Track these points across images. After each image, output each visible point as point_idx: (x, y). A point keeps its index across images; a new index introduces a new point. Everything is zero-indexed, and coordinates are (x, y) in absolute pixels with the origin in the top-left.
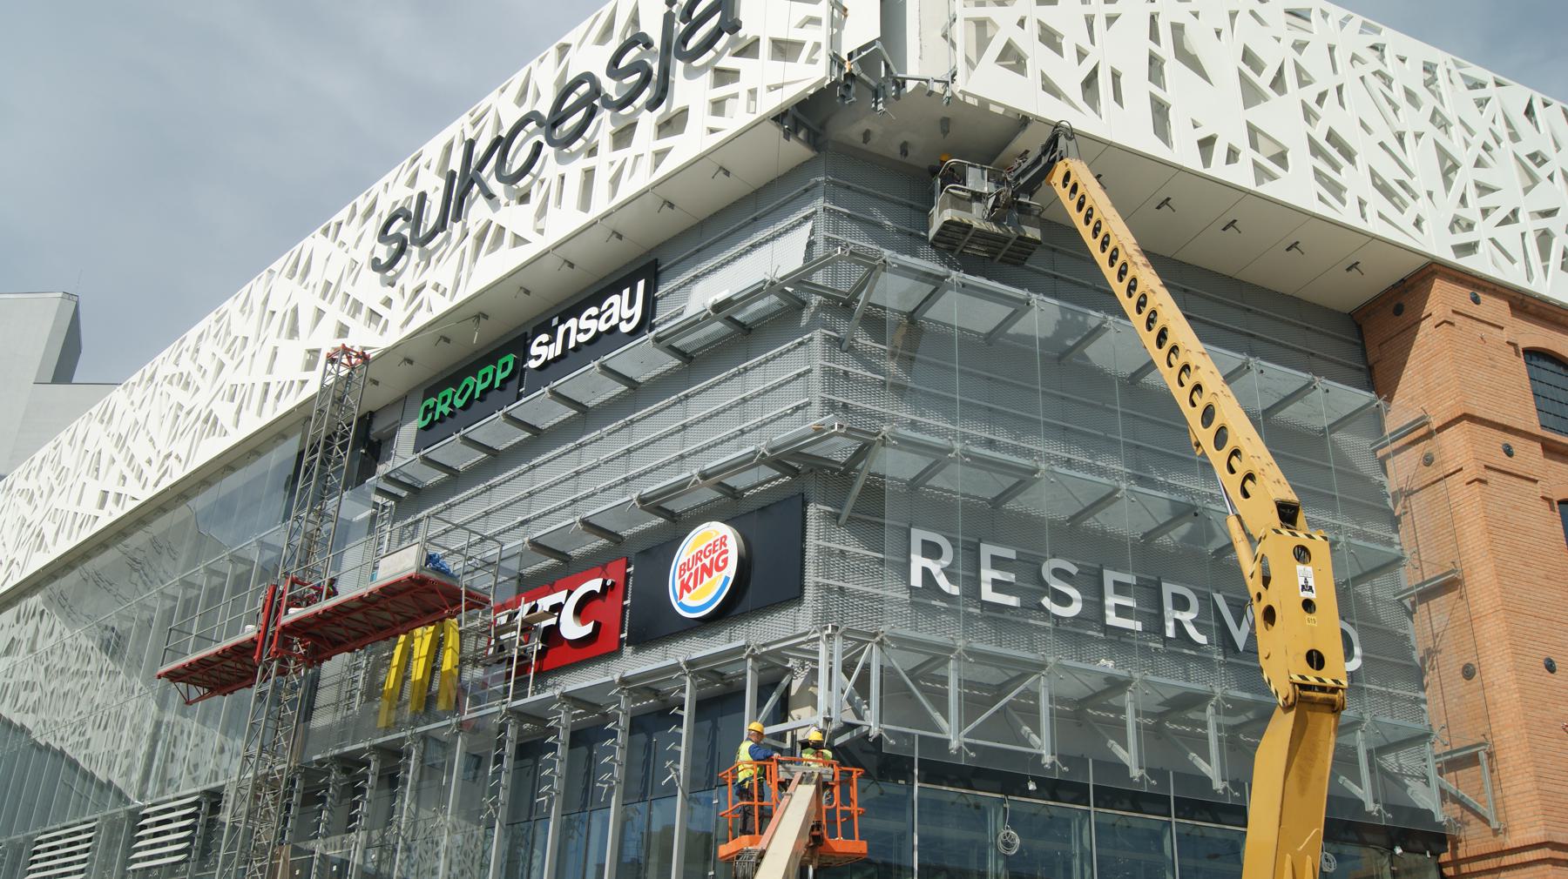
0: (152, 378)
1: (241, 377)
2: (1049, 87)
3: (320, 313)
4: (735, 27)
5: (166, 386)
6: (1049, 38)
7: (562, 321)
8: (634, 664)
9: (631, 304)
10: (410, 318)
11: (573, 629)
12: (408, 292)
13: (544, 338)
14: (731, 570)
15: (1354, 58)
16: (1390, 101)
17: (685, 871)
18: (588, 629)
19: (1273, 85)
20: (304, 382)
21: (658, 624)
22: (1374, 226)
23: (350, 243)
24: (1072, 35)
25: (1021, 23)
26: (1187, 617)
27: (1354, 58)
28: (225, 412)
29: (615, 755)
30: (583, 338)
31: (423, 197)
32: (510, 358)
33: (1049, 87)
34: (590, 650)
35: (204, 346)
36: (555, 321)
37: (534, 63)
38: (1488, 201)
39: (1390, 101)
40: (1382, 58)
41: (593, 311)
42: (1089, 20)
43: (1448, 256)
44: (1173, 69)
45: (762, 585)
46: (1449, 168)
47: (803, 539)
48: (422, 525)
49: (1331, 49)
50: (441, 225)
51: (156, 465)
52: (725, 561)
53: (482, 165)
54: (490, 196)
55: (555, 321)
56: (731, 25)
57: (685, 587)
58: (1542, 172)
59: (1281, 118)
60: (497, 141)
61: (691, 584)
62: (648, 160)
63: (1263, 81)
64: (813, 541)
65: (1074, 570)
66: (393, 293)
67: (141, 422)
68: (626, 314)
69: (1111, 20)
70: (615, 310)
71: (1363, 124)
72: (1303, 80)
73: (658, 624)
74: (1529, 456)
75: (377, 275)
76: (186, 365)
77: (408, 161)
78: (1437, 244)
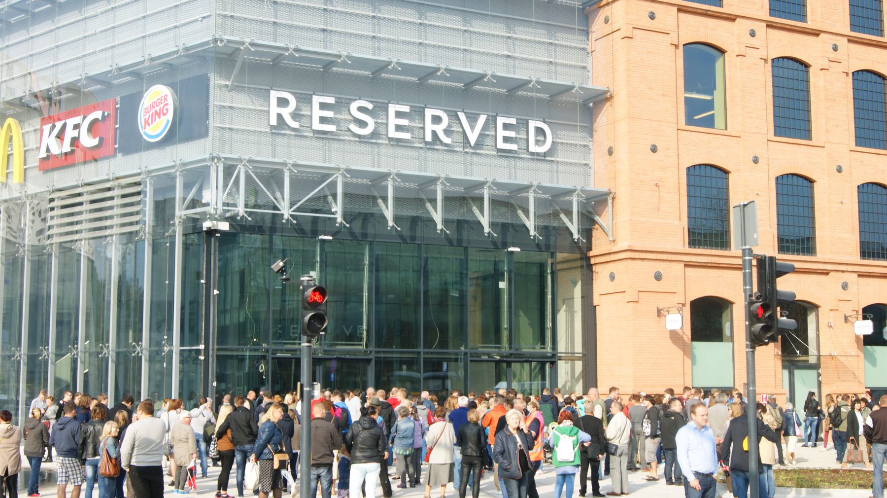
8: (122, 166)
14: (170, 116)
17: (883, 257)
18: (95, 142)
21: (132, 142)
29: (85, 213)
34: (93, 156)
45: (188, 125)
47: (208, 101)
52: (167, 110)
57: (147, 122)
61: (150, 121)
65: (370, 106)
73: (132, 142)
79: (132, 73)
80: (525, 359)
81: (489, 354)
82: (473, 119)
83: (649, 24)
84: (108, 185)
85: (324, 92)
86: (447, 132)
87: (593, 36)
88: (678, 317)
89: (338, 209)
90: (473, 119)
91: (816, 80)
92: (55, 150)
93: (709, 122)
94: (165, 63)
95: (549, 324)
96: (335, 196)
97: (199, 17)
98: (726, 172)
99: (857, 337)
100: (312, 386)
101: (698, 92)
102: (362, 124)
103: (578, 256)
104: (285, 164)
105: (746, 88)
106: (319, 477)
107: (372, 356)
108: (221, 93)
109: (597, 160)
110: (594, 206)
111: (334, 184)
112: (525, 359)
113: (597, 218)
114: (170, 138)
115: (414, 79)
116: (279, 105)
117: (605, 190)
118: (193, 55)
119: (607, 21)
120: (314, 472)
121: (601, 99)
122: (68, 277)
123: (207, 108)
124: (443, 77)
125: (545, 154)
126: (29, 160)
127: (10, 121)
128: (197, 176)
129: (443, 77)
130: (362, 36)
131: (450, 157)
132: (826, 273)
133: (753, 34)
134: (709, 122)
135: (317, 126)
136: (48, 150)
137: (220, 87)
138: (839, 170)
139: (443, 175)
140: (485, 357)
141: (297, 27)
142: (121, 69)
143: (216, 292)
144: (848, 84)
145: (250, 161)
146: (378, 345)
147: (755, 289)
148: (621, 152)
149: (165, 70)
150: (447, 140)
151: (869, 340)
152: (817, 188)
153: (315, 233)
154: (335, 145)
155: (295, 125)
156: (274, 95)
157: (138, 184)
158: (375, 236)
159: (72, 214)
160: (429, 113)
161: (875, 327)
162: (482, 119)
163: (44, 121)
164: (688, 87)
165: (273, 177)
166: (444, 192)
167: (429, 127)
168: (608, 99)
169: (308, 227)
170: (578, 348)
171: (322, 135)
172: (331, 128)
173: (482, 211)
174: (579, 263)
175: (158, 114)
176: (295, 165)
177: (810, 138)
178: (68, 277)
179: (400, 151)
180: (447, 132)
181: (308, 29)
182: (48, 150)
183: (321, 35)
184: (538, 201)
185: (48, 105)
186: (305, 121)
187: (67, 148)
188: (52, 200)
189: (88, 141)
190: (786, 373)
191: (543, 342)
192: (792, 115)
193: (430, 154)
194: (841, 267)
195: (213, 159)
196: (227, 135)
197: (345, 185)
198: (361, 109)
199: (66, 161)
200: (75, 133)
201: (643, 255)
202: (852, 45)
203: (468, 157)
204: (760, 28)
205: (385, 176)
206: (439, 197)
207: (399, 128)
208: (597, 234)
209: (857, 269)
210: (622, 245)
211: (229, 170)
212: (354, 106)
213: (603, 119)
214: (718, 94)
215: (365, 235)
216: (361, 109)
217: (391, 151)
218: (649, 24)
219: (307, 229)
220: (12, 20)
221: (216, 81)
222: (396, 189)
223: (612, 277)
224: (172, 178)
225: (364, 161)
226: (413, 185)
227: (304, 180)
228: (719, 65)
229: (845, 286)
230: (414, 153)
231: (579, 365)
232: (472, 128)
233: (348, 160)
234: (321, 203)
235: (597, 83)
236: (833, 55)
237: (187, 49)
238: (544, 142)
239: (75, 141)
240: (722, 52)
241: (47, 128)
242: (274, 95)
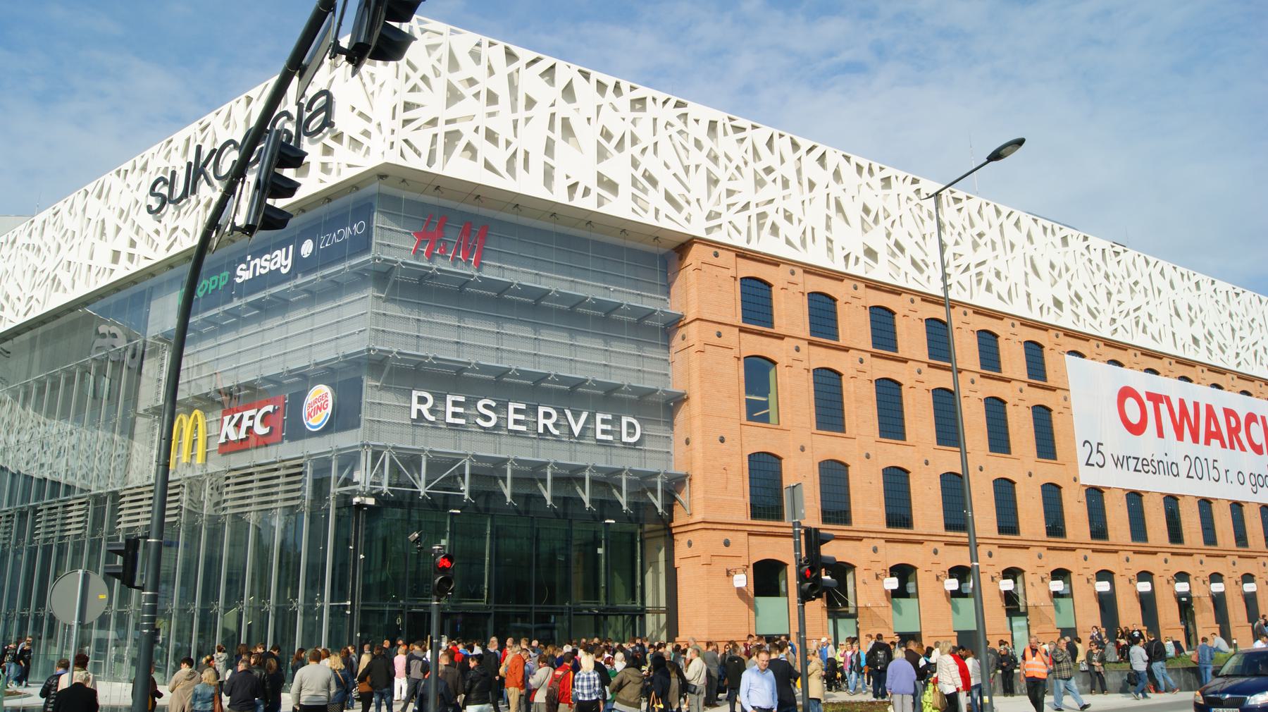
0: (14, 242)
1: (71, 256)
2: (488, 166)
3: (118, 229)
4: (331, 125)
5: (24, 251)
6: (491, 136)
7: (253, 259)
9: (286, 258)
10: (172, 245)
11: (260, 430)
13: (243, 266)
14: (329, 410)
15: (668, 124)
16: (685, 148)
18: (266, 430)
19: (616, 147)
20: (112, 270)
21: (297, 431)
22: (664, 223)
23: (134, 187)
24: (504, 132)
25: (476, 130)
27: (668, 124)
28: (65, 277)
30: (263, 271)
31: (174, 173)
33: (488, 166)
34: (264, 442)
35: (48, 229)
37: (233, 102)
39: (685, 148)
40: (685, 123)
41: (267, 257)
42: (515, 122)
43: (703, 235)
44: (560, 145)
45: (343, 418)
46: (713, 182)
49: (655, 120)
50: (185, 195)
51: (24, 301)
53: (205, 164)
54: (209, 183)
55: (249, 258)
56: (328, 123)
57: (309, 415)
58: (769, 179)
59: (617, 167)
60: (213, 151)
63: (610, 146)
65: (494, 404)
66: (160, 227)
67: (10, 271)
68: (284, 263)
69: (528, 120)
71: (665, 164)
72: (634, 141)
73: (297, 431)
75: (151, 216)
76: (36, 239)
77: (165, 142)
78: (696, 228)
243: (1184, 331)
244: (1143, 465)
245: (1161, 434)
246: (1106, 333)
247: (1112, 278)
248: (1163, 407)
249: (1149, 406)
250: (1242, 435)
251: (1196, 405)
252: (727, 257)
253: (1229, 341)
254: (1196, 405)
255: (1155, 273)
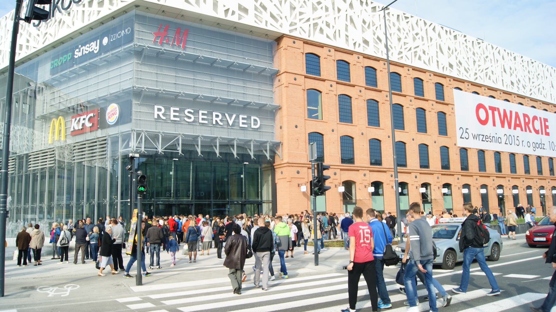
7: (82, 47)
8: (99, 133)
9: (96, 46)
12: (43, 34)
13: (77, 50)
14: (117, 115)
18: (91, 125)
22: (270, 28)
26: (218, 119)
30: (87, 52)
32: (70, 54)
36: (80, 46)
38: (302, 17)
47: (131, 109)
48: (56, 93)
53: (58, 3)
54: (60, 12)
55: (80, 46)
57: (109, 117)
62: (96, 13)
64: (134, 109)
65: (192, 111)
66: (39, 33)
70: (93, 46)
74: (301, 80)
78: (285, 30)
79: (103, 100)
80: (251, 203)
81: (237, 202)
82: (231, 116)
83: (294, 82)
84: (95, 141)
85: (175, 106)
86: (164, 115)
87: (275, 86)
88: (305, 187)
89: (180, 149)
90: (231, 116)
91: (354, 103)
92: (76, 128)
93: (317, 117)
94: (116, 96)
95: (260, 190)
96: (179, 144)
97: (128, 78)
98: (323, 135)
99: (369, 193)
100: (142, 213)
101: (313, 107)
102: (190, 118)
103: (270, 165)
104: (160, 132)
105: (329, 106)
106: (155, 248)
107: (194, 203)
108: (136, 107)
109: (277, 131)
110: (276, 146)
111: (178, 140)
112: (251, 203)
113: (277, 152)
114: (117, 123)
115: (209, 101)
116: (158, 111)
117: (279, 141)
118: (125, 92)
119: (279, 81)
120: (153, 246)
121: (279, 108)
122: (91, 176)
123: (131, 112)
124: (219, 101)
125: (257, 129)
126: (67, 131)
127: (60, 117)
128: (126, 138)
129: (219, 101)
130: (189, 86)
131: (223, 130)
132: (358, 170)
133: (331, 86)
134: (317, 117)
135: (172, 118)
136: (74, 128)
137: (136, 104)
138: (362, 134)
139: (219, 136)
140: (236, 203)
141: (165, 82)
142: (99, 98)
143: (134, 180)
144: (415, 112)
145: (146, 131)
146: (195, 199)
147: (316, 175)
148: (285, 128)
149: (115, 98)
150: (221, 124)
151: (374, 194)
152: (355, 140)
153: (172, 158)
154: (180, 125)
155: (164, 118)
156: (156, 107)
157: (105, 140)
158: (194, 159)
159: (83, 151)
160: (214, 114)
161: (375, 189)
162: (234, 116)
163: (73, 118)
164: (309, 104)
165: (155, 137)
166: (219, 142)
167: (214, 119)
168: (280, 109)
169: (169, 155)
170: (271, 199)
171: (243, 129)
172: (178, 119)
173: (234, 150)
174: (270, 168)
175: (113, 114)
176: (163, 133)
177: (352, 123)
178: (91, 176)
179: (204, 128)
180: (164, 115)
181: (169, 83)
182: (74, 128)
183: (174, 85)
184: (254, 146)
185: (75, 111)
186: (168, 117)
187: (80, 127)
188: (75, 146)
189: (88, 125)
190: (344, 206)
191: (258, 197)
192: (346, 115)
193: (215, 129)
194: (363, 168)
195: (132, 130)
196: (138, 122)
197: (182, 140)
198: (189, 112)
199: (82, 131)
200: (83, 122)
201: (293, 165)
202: (366, 90)
203: (230, 130)
204: (334, 84)
205: (216, 138)
206: (218, 145)
207: (203, 119)
208: (276, 157)
209: (369, 169)
210: (285, 161)
211: (138, 135)
212: (186, 111)
213: (278, 117)
214: (320, 107)
215: (191, 158)
216: (189, 112)
217: (252, 132)
218: (294, 82)
219: (169, 155)
220: (62, 80)
221: (134, 102)
222: (201, 141)
223: (282, 173)
224: (118, 137)
225: (190, 132)
226: (209, 140)
227: (166, 139)
228: (320, 97)
229: (365, 175)
230: (209, 129)
231: (271, 204)
232: (231, 119)
233: (183, 131)
234: (174, 147)
235: (276, 103)
236: (360, 94)
237: (123, 90)
238: (257, 124)
239: (83, 125)
240: (321, 92)
241: (74, 120)
242: (156, 107)
243: (507, 79)
244: (486, 138)
245: (494, 125)
246: (472, 79)
247: (476, 55)
248: (496, 113)
249: (490, 112)
250: (531, 125)
251: (511, 112)
252: (299, 44)
253: (527, 84)
254: (511, 112)
255: (545, 70)
